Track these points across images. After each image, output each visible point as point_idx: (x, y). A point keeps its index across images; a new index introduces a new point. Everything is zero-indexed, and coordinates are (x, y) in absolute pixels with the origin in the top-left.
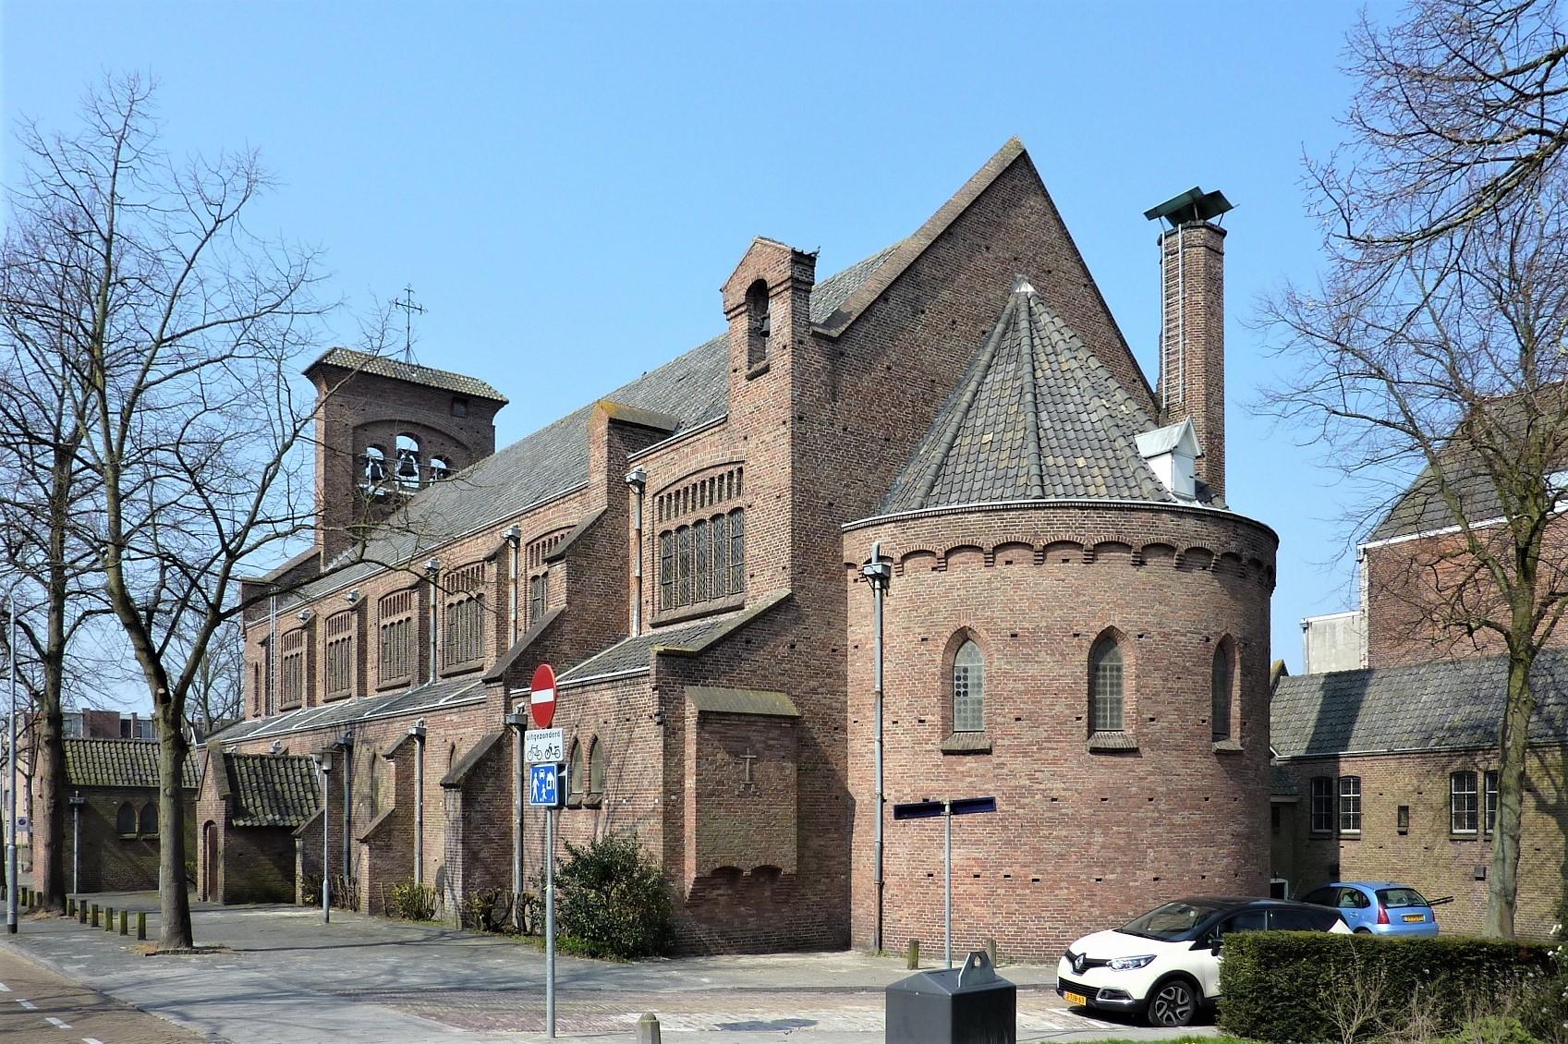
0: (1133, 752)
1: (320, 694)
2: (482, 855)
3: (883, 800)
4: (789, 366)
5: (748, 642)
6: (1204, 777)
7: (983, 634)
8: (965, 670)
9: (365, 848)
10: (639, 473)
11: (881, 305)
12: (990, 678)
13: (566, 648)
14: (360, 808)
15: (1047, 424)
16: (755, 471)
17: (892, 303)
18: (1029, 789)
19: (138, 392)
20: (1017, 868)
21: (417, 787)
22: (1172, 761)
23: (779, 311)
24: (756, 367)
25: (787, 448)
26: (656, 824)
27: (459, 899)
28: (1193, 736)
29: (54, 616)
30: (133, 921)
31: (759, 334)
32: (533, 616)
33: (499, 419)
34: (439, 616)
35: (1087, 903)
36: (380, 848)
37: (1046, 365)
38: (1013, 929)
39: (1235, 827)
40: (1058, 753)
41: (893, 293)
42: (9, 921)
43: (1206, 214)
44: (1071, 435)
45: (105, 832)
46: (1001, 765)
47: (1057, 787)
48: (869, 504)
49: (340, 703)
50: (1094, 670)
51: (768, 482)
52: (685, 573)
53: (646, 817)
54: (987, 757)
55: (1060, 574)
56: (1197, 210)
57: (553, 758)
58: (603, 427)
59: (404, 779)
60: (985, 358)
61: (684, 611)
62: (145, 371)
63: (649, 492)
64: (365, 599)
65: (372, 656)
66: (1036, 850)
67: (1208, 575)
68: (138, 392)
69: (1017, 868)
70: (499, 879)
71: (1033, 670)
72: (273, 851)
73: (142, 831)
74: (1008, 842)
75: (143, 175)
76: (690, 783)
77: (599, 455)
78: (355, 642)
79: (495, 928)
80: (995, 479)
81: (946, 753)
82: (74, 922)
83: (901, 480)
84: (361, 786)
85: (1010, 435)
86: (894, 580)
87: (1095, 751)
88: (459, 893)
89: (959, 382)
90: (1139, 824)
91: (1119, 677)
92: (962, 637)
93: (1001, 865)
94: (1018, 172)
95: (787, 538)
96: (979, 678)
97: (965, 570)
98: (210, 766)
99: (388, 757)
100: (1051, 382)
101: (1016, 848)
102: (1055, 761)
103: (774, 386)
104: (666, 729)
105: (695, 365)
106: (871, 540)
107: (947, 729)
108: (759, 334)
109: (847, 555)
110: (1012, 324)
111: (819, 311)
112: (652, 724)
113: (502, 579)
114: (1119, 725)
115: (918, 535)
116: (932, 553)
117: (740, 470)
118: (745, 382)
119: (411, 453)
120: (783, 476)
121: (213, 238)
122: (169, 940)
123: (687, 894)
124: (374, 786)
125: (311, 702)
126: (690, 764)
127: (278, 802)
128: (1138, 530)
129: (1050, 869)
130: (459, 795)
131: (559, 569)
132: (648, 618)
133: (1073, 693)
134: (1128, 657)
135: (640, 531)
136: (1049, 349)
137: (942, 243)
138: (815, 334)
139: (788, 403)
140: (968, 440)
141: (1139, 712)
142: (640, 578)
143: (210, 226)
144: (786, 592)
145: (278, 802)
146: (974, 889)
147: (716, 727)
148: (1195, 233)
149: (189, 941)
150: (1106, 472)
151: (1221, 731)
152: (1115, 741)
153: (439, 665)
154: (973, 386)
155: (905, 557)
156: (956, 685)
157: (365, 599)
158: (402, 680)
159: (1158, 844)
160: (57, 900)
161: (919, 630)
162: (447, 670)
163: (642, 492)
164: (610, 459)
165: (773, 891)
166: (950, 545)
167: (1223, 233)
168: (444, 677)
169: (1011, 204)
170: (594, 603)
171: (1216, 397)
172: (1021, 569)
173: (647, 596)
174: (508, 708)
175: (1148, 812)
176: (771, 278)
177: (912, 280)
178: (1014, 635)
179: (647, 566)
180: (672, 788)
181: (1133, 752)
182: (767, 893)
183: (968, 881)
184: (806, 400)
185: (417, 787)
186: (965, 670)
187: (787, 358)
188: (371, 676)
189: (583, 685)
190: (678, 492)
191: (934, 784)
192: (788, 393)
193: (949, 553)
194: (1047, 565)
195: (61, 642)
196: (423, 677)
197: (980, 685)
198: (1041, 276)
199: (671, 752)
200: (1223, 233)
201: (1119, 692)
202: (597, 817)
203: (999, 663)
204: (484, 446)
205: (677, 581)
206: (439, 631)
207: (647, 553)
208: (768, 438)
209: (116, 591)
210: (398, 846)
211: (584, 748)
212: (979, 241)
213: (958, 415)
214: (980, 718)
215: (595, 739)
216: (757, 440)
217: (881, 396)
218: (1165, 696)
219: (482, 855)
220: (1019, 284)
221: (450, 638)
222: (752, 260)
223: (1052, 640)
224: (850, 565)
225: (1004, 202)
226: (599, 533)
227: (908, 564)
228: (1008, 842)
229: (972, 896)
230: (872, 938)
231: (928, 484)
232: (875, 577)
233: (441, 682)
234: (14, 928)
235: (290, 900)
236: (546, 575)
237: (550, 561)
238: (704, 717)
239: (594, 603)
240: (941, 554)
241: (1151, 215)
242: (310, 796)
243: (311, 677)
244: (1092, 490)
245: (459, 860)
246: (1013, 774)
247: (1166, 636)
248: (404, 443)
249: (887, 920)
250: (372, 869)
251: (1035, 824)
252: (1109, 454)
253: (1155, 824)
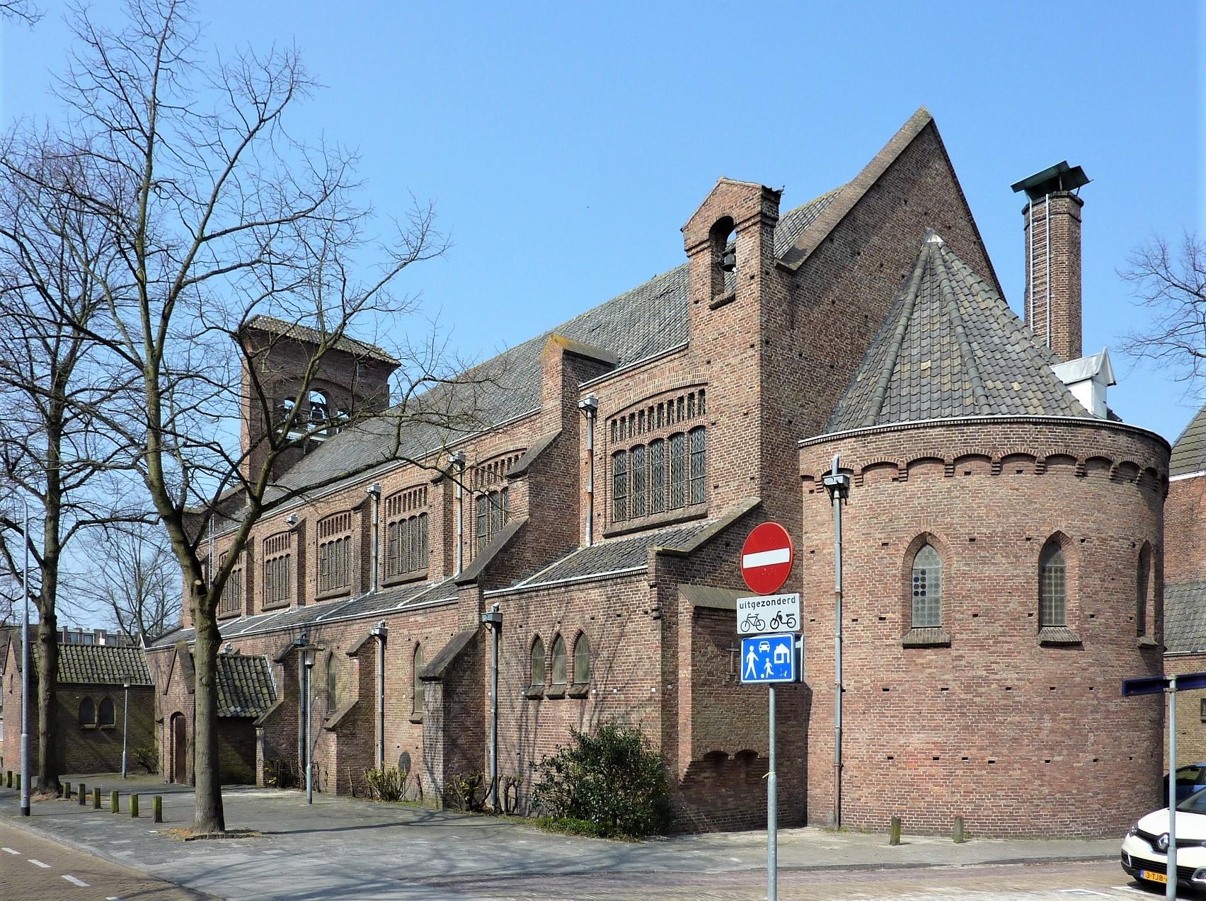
0: (1077, 645)
1: (258, 605)
2: (459, 742)
3: (843, 691)
4: (757, 294)
5: (727, 545)
6: (1131, 668)
7: (943, 538)
8: (923, 572)
9: (333, 736)
10: (592, 398)
11: (828, 244)
12: (949, 579)
13: (528, 555)
14: (316, 703)
15: (980, 353)
16: (720, 391)
17: (836, 243)
18: (985, 679)
19: (179, 287)
20: (974, 751)
21: (378, 681)
22: (1108, 653)
23: (745, 245)
24: (718, 299)
25: (756, 370)
26: (653, 712)
27: (440, 783)
28: (1123, 631)
29: (50, 525)
30: (147, 803)
31: (722, 267)
32: (477, 532)
33: (392, 380)
34: (381, 533)
35: (1038, 782)
36: (346, 736)
37: (966, 304)
38: (970, 807)
39: (1151, 713)
40: (1012, 646)
41: (837, 235)
42: (23, 804)
43: (1068, 187)
44: (1002, 362)
45: (83, 722)
46: (960, 657)
47: (1011, 677)
48: (819, 423)
49: (281, 611)
50: (1042, 570)
51: (734, 400)
52: (637, 488)
53: (642, 705)
54: (945, 650)
55: (1016, 483)
56: (1059, 183)
57: (783, 628)
58: (557, 358)
59: (366, 674)
60: (911, 297)
61: (637, 522)
62: (186, 267)
63: (602, 416)
64: (304, 521)
65: (311, 570)
66: (992, 734)
67: (1134, 487)
68: (179, 287)
69: (974, 751)
70: (474, 764)
71: (989, 571)
72: (245, 742)
73: (101, 722)
74: (966, 728)
75: (180, 79)
76: (685, 673)
77: (552, 385)
78: (244, 573)
79: (476, 808)
80: (941, 400)
81: (906, 646)
82: (73, 803)
83: (843, 403)
84: (316, 679)
85: (947, 362)
86: (853, 490)
87: (1045, 644)
88: (439, 776)
89: (885, 318)
90: (1082, 711)
91: (1062, 578)
92: (922, 541)
93: (958, 749)
94: (927, 136)
95: (755, 451)
96: (937, 579)
97: (926, 480)
98: (178, 664)
99: (351, 655)
100: (974, 318)
101: (973, 733)
102: (1009, 653)
103: (741, 314)
104: (663, 623)
105: (603, 319)
106: (830, 454)
107: (906, 627)
108: (722, 267)
109: (804, 468)
110: (929, 269)
111: (782, 242)
112: (648, 619)
113: (448, 499)
114: (1062, 621)
115: (879, 449)
116: (894, 465)
117: (702, 393)
118: (707, 312)
119: (322, 406)
120: (750, 392)
121: (254, 141)
122: (204, 825)
123: (681, 777)
124: (331, 681)
125: (250, 611)
126: (685, 656)
127: (243, 700)
128: (1082, 444)
129: (1005, 751)
130: (439, 688)
131: (521, 486)
132: (600, 530)
133: (1026, 592)
134: (1071, 559)
135: (591, 451)
136: (966, 291)
137: (873, 193)
138: (779, 267)
139: (757, 328)
140: (907, 367)
141: (1082, 609)
142: (592, 494)
143: (253, 124)
144: (755, 500)
145: (243, 700)
146: (933, 770)
147: (707, 622)
148: (1060, 202)
149: (221, 825)
150: (1039, 395)
151: (1141, 631)
152: (1061, 636)
153: (380, 575)
154: (903, 321)
155: (866, 469)
156: (916, 586)
157: (304, 521)
158: (341, 590)
159: (1097, 729)
160: (51, 784)
161: (880, 536)
162: (388, 581)
163: (594, 416)
164: (564, 387)
165: (748, 774)
166: (911, 457)
167: (1081, 203)
168: (385, 586)
169: (923, 165)
170: (551, 515)
171: (1076, 344)
172: (978, 479)
173: (599, 509)
174: (482, 608)
175: (1087, 700)
176: (737, 215)
177: (853, 223)
178: (972, 540)
179: (599, 483)
180: (669, 678)
181: (1077, 645)
182: (743, 776)
183: (927, 763)
184: (772, 326)
185: (378, 681)
186: (923, 572)
187: (756, 286)
188: (310, 588)
189: (567, 585)
190: (632, 416)
191: (894, 676)
192: (756, 320)
193: (911, 464)
194: (1003, 476)
195: (56, 549)
196: (365, 588)
197: (937, 586)
198: (945, 229)
199: (668, 645)
200: (1081, 203)
201: (1062, 592)
202: (583, 706)
203: (958, 565)
204: (378, 405)
205: (630, 495)
206: (381, 547)
207: (598, 471)
208: (733, 361)
209: (156, 483)
210: (362, 735)
211: (568, 643)
212: (900, 194)
213: (894, 347)
214: (937, 615)
215: (581, 633)
216: (728, 363)
217: (827, 327)
218: (1103, 595)
219: (459, 742)
220: (928, 234)
221: (390, 554)
222: (717, 200)
223: (1007, 544)
224: (806, 478)
225: (917, 162)
226: (555, 452)
227: (868, 475)
228: (966, 728)
229: (931, 776)
230: (830, 816)
231: (878, 404)
232: (832, 489)
233: (381, 591)
234: (27, 811)
235: (252, 781)
236: (506, 489)
237: (513, 477)
238: (700, 613)
239: (551, 515)
240: (902, 465)
241: (1016, 188)
242: (265, 691)
243: (250, 590)
244: (1031, 409)
245: (440, 746)
246: (970, 666)
247: (1103, 541)
248: (317, 398)
249: (846, 799)
250: (340, 755)
251: (991, 711)
252: (1038, 380)
253: (1095, 711)
